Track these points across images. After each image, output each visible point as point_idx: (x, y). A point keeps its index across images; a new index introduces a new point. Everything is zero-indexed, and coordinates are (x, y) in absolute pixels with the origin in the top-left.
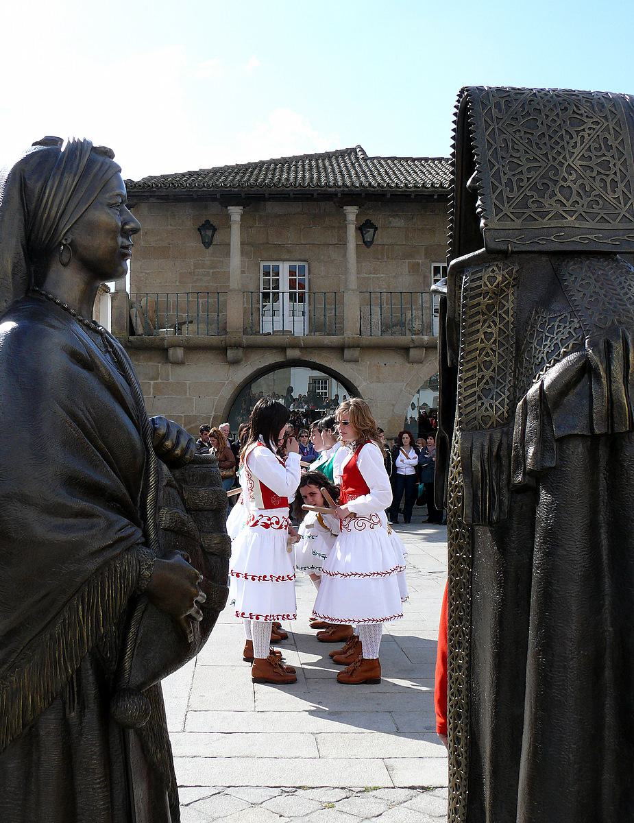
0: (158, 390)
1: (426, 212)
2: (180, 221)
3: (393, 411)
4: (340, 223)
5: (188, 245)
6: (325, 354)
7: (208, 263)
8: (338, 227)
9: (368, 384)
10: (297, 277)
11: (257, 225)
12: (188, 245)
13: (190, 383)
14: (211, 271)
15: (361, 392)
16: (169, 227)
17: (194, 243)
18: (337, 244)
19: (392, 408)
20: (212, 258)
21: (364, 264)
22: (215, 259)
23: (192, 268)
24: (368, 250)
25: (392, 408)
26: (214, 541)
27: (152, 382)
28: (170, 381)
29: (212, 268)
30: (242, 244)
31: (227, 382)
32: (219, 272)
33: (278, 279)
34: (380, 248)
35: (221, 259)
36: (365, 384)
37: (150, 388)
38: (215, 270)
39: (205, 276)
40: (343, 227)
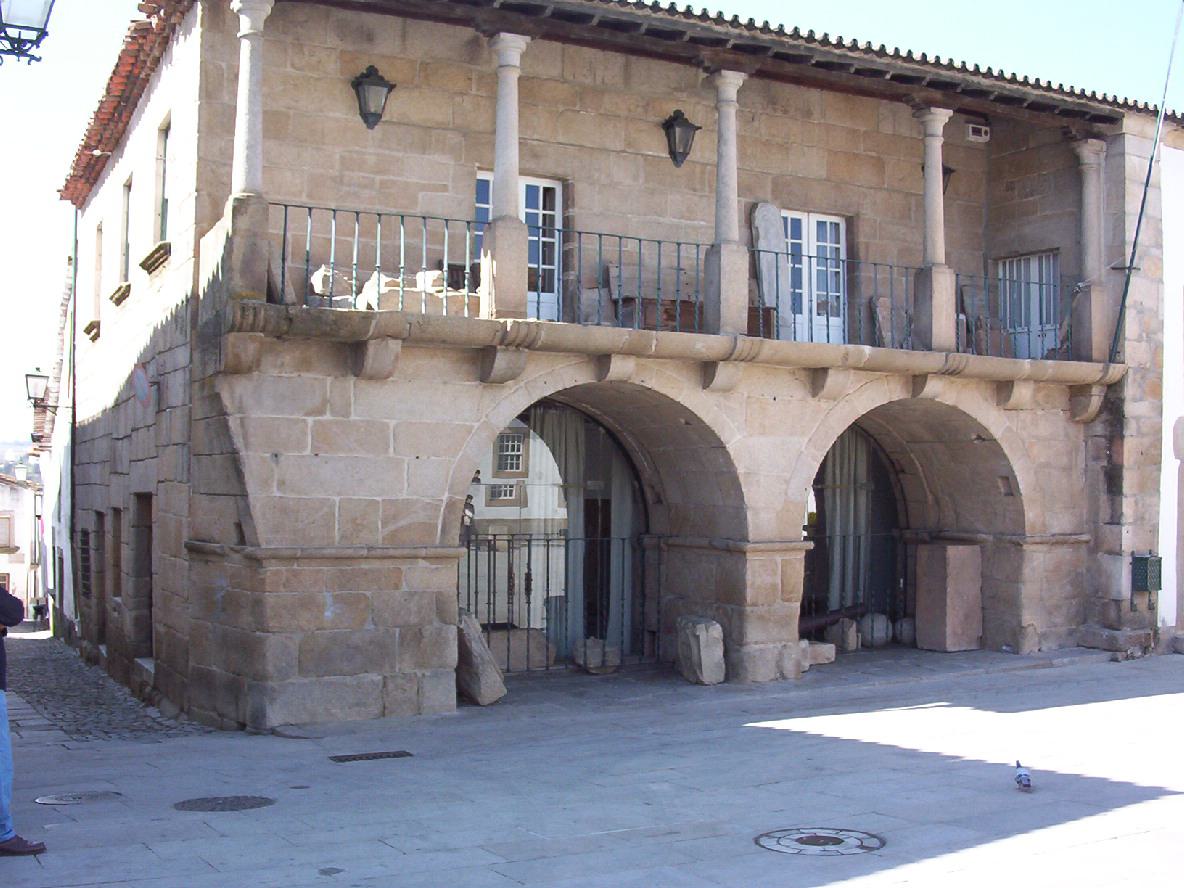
0: (324, 440)
1: (775, 110)
2: (315, 59)
3: (786, 494)
4: (630, 110)
5: (331, 114)
6: (669, 373)
7: (371, 160)
8: (627, 118)
9: (744, 437)
10: (541, 212)
11: (474, 92)
12: (331, 114)
13: (396, 426)
14: (378, 178)
15: (732, 453)
16: (289, 69)
17: (341, 111)
18: (624, 151)
19: (784, 487)
20: (380, 151)
21: (670, 197)
22: (387, 152)
23: (337, 166)
24: (678, 171)
25: (784, 487)
26: (808, 573)
27: (310, 420)
28: (353, 417)
29: (378, 172)
30: (738, 169)
31: (476, 425)
32: (394, 182)
33: (792, 219)
34: (698, 169)
35: (400, 154)
36: (739, 437)
37: (306, 434)
38: (386, 177)
39: (365, 187)
40: (491, 84)
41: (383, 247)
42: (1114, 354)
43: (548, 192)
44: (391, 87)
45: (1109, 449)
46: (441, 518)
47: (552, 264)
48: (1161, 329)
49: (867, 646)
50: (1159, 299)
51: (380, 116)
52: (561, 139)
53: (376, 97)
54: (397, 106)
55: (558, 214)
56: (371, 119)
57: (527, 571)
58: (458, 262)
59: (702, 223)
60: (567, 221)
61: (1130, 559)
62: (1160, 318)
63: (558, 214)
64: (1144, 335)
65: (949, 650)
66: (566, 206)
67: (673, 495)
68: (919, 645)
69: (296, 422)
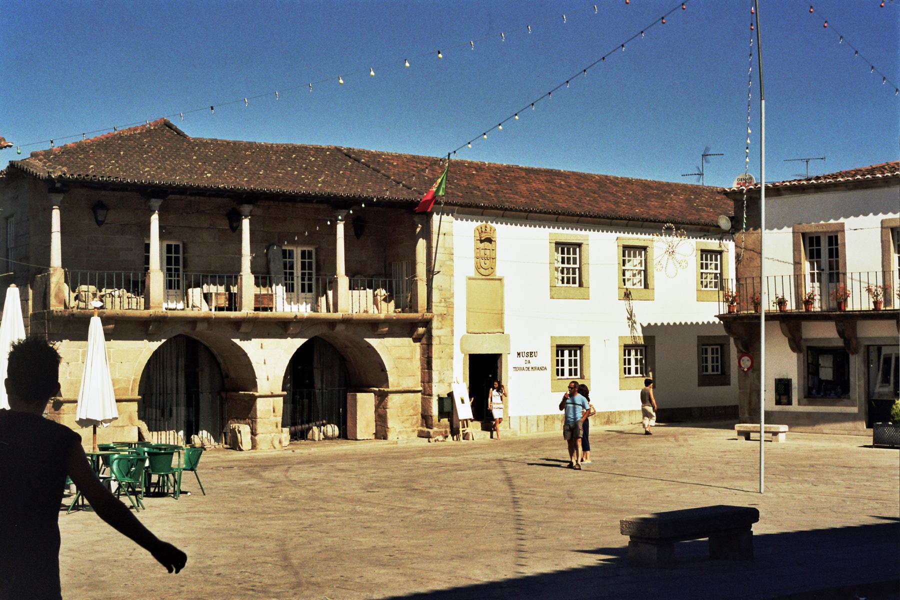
27: (81, 350)
31: (144, 350)
41: (124, 275)
42: (429, 308)
43: (177, 247)
44: (108, 209)
45: (428, 350)
46: (131, 385)
47: (312, 270)
48: (452, 296)
49: (326, 438)
50: (451, 284)
51: (104, 221)
52: (181, 225)
53: (101, 213)
54: (112, 216)
55: (181, 256)
56: (100, 223)
57: (771, 434)
58: (136, 280)
60: (185, 259)
61: (437, 398)
62: (452, 292)
63: (181, 256)
64: (443, 300)
65: (358, 438)
66: (184, 253)
67: (232, 374)
68: (349, 438)
69: (76, 351)
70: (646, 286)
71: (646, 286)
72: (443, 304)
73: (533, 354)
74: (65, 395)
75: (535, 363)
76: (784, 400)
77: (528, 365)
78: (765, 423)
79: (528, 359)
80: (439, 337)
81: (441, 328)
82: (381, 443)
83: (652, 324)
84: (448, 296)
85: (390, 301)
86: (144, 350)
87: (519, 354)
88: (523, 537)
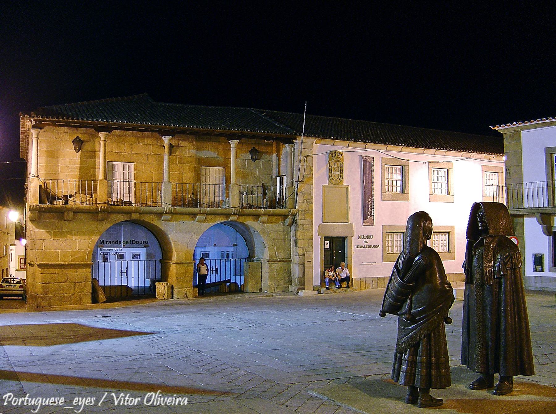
16: (55, 139)
18: (151, 154)
31: (96, 232)
59: (176, 172)
64: (305, 201)
70: (448, 194)
71: (448, 194)
72: (305, 203)
73: (370, 237)
74: (406, 224)
75: (370, 242)
76: (539, 268)
77: (366, 244)
78: (124, 259)
79: (366, 240)
80: (303, 225)
81: (304, 219)
82: (9, 245)
83: (469, 218)
84: (309, 197)
85: (500, 136)
86: (96, 232)
87: (359, 237)
88: (124, 271)
